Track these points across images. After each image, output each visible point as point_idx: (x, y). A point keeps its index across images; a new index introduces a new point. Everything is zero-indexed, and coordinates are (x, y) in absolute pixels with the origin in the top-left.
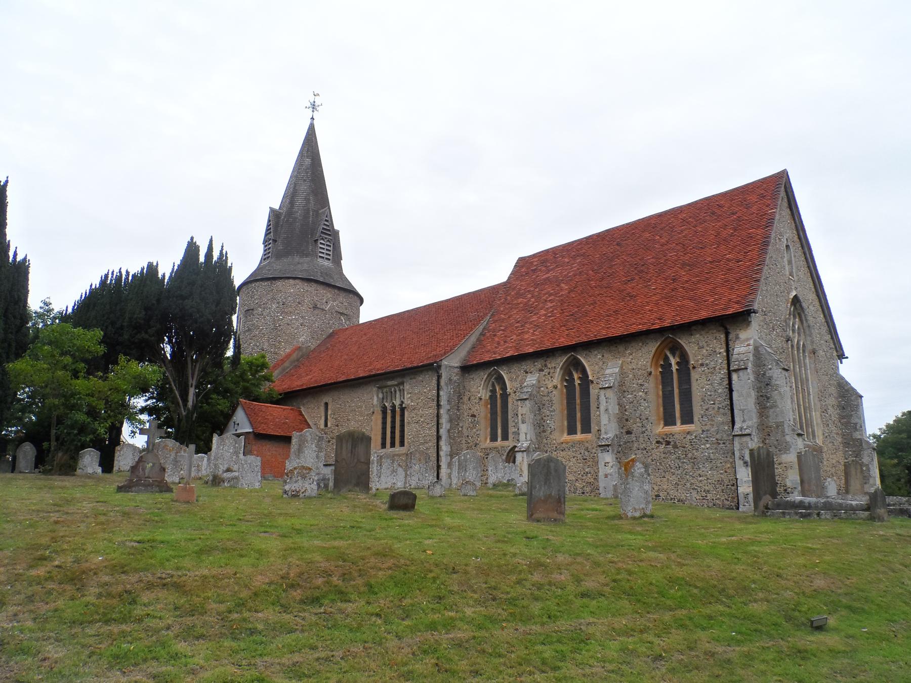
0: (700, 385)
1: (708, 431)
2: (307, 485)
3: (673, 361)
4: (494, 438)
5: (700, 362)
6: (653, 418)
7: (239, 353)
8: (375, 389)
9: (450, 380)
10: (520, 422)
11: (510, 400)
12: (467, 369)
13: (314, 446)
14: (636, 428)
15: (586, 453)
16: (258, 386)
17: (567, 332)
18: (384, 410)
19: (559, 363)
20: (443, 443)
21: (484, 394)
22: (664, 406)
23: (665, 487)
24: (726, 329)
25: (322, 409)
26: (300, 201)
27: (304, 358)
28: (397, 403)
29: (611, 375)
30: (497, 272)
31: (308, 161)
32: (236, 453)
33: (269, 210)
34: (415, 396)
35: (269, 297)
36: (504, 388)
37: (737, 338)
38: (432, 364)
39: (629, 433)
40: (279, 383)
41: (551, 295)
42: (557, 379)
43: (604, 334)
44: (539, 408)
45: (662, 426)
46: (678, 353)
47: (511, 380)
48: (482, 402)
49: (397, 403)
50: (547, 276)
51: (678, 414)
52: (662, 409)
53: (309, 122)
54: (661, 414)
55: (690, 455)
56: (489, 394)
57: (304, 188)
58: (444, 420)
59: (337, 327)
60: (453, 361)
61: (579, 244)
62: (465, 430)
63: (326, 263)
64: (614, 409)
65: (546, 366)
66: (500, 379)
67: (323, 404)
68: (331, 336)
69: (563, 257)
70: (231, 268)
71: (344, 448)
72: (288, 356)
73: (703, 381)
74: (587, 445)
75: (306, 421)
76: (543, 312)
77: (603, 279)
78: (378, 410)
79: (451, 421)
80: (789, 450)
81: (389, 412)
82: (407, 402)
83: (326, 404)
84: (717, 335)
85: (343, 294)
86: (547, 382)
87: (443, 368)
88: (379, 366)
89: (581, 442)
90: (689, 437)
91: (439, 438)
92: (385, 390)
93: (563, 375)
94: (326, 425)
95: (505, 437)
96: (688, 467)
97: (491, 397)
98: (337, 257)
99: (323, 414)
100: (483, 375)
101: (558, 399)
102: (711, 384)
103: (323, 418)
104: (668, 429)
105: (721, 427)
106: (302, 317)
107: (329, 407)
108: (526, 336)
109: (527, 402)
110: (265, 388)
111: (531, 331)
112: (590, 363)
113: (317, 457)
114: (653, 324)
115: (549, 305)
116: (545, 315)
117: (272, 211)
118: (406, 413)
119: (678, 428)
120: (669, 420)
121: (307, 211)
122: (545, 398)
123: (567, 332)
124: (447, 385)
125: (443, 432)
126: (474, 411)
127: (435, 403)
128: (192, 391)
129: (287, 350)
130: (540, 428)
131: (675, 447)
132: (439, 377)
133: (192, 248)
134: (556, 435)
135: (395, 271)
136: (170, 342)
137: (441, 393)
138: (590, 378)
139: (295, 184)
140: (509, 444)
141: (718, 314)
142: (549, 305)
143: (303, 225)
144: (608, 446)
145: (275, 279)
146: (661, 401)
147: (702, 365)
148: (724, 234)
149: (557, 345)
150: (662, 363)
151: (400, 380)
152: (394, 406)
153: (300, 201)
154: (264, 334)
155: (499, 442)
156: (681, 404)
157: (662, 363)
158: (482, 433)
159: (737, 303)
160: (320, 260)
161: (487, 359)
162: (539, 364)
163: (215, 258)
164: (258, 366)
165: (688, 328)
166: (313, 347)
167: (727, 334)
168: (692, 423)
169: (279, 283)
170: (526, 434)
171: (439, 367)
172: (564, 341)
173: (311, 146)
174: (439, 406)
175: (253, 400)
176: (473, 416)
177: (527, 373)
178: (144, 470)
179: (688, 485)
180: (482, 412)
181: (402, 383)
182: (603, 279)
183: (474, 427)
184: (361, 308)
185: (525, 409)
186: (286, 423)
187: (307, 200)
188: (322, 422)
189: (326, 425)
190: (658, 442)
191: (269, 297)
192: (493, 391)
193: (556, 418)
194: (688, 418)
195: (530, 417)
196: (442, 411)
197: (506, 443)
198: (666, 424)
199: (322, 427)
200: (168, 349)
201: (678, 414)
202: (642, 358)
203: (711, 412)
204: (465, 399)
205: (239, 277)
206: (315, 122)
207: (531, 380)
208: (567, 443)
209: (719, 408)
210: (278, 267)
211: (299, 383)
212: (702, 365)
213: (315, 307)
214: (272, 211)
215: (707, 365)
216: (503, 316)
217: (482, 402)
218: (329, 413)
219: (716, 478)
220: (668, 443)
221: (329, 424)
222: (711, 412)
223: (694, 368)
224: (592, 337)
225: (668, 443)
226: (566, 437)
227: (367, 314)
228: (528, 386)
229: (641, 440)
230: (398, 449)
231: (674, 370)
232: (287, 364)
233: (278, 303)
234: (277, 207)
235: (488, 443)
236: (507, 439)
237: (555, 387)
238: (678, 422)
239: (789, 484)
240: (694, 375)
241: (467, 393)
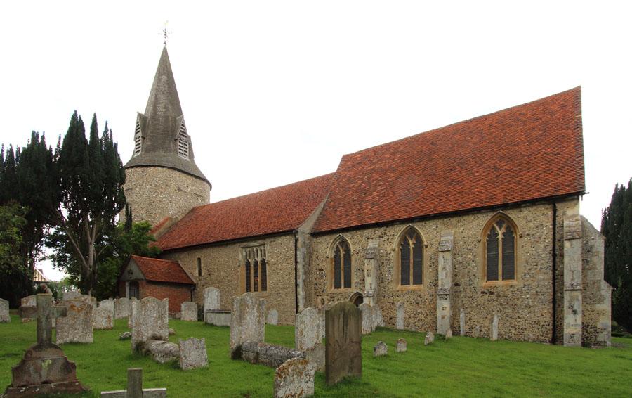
0: (523, 250)
1: (529, 285)
2: (304, 385)
3: (500, 232)
4: (338, 286)
5: (527, 233)
6: (480, 274)
7: (131, 220)
8: (240, 249)
9: (304, 243)
10: (366, 275)
11: (353, 258)
12: (315, 234)
13: (255, 311)
14: (463, 281)
15: (419, 299)
16: (146, 243)
17: (402, 209)
18: (248, 265)
19: (399, 230)
20: (300, 290)
21: (330, 253)
22: (488, 266)
23: (487, 325)
24: (555, 206)
25: (196, 262)
26: (161, 109)
27: (175, 226)
28: (259, 260)
29: (447, 241)
30: (330, 166)
31: (164, 78)
32: (161, 317)
33: (137, 114)
34: (277, 253)
35: (143, 180)
36: (347, 250)
37: (564, 214)
38: (292, 231)
39: (457, 285)
40: (161, 246)
41: (380, 181)
42: (395, 243)
43: (439, 210)
44: (380, 265)
45: (485, 280)
46: (344, 246)
47: (354, 244)
48: (329, 260)
49: (259, 260)
50: (371, 167)
51: (500, 272)
52: (486, 268)
53: (163, 46)
54: (486, 272)
55: (511, 303)
56: (333, 254)
57: (162, 98)
58: (301, 273)
59: (196, 205)
60: (306, 228)
61: (395, 145)
62: (314, 280)
63: (184, 158)
64: (449, 267)
65: (385, 233)
66: (344, 243)
67: (196, 259)
68: (193, 210)
69: (383, 154)
70: (116, 145)
71: (336, 328)
72: (162, 224)
73: (528, 248)
74: (419, 293)
75: (183, 270)
76: (375, 193)
77: (425, 169)
78: (243, 264)
79: (305, 273)
80: (603, 301)
81: (252, 265)
82: (267, 259)
83: (199, 259)
84: (545, 212)
85: (198, 180)
86: (386, 246)
87: (299, 233)
88: (241, 233)
89: (415, 291)
90: (511, 289)
91: (297, 285)
92: (248, 250)
93: (400, 241)
94: (200, 274)
95: (348, 285)
96: (509, 311)
97: (335, 257)
98: (191, 156)
99: (197, 266)
100: (329, 239)
101: (394, 258)
102: (536, 250)
103: (197, 269)
104: (491, 283)
105: (542, 283)
106: (171, 196)
107: (202, 261)
108: (366, 211)
109: (373, 261)
110: (149, 245)
111: (369, 207)
112: (427, 231)
113: (259, 322)
114: (486, 202)
115: (380, 188)
116: (378, 196)
117: (140, 115)
118: (268, 267)
119: (500, 283)
120: (338, 286)
121: (167, 118)
122: (385, 258)
123: (402, 209)
124: (302, 247)
125: (300, 281)
126: (321, 266)
127: (293, 260)
128: (92, 248)
129: (161, 220)
130: (381, 280)
131: (498, 296)
132: (297, 240)
133: (76, 124)
134: (392, 285)
135: (241, 157)
136: (66, 206)
137: (298, 253)
138: (425, 243)
139: (156, 96)
140: (353, 290)
141: (550, 194)
142: (380, 188)
143: (163, 127)
144: (446, 295)
145: (147, 166)
146: (400, 257)
147: (528, 235)
148: (534, 134)
149: (397, 218)
150: (489, 233)
151: (261, 242)
152: (256, 263)
153: (161, 109)
154: (150, 201)
155: (342, 289)
156: (503, 265)
157: (489, 233)
158: (328, 283)
159: (568, 186)
160: (180, 155)
161: (334, 228)
162: (380, 231)
163: (100, 135)
164: (144, 229)
165: (517, 205)
166: (179, 218)
167: (555, 211)
168: (514, 279)
169: (151, 170)
170: (371, 284)
171: (297, 232)
172: (402, 215)
173: (165, 68)
174: (296, 262)
175: (141, 255)
176: (321, 270)
177: (368, 239)
178: (38, 370)
179: (508, 324)
180: (328, 267)
181: (264, 245)
182: (425, 169)
183: (322, 278)
184: (211, 192)
185: (370, 266)
186: (169, 272)
187: (166, 107)
188: (197, 272)
189: (200, 274)
190: (482, 293)
191: (143, 180)
192: (337, 252)
193: (393, 273)
194: (509, 274)
195: (373, 272)
196: (299, 266)
197: (349, 290)
198: (489, 279)
199: (197, 275)
200: (65, 213)
201: (500, 272)
202: (474, 228)
203: (533, 271)
204: (314, 257)
205: (126, 150)
206: (167, 47)
207: (373, 244)
208: (402, 291)
209: (541, 268)
210: (148, 158)
211: (175, 243)
212: (528, 235)
213: (179, 189)
214: (140, 115)
215: (533, 235)
216: (339, 197)
217: (329, 260)
218: (202, 265)
219: (533, 319)
220: (492, 293)
221: (203, 274)
222: (533, 271)
223: (521, 237)
224: (429, 212)
225: (492, 293)
226: (400, 287)
227: (216, 197)
228: (371, 248)
229: (468, 291)
230: (260, 293)
231: (500, 239)
232: (162, 230)
233: (151, 185)
234: (143, 112)
235: (333, 290)
236: (266, 290)
237: (393, 250)
238: (500, 277)
239: (599, 326)
240: (520, 243)
241: (315, 253)
